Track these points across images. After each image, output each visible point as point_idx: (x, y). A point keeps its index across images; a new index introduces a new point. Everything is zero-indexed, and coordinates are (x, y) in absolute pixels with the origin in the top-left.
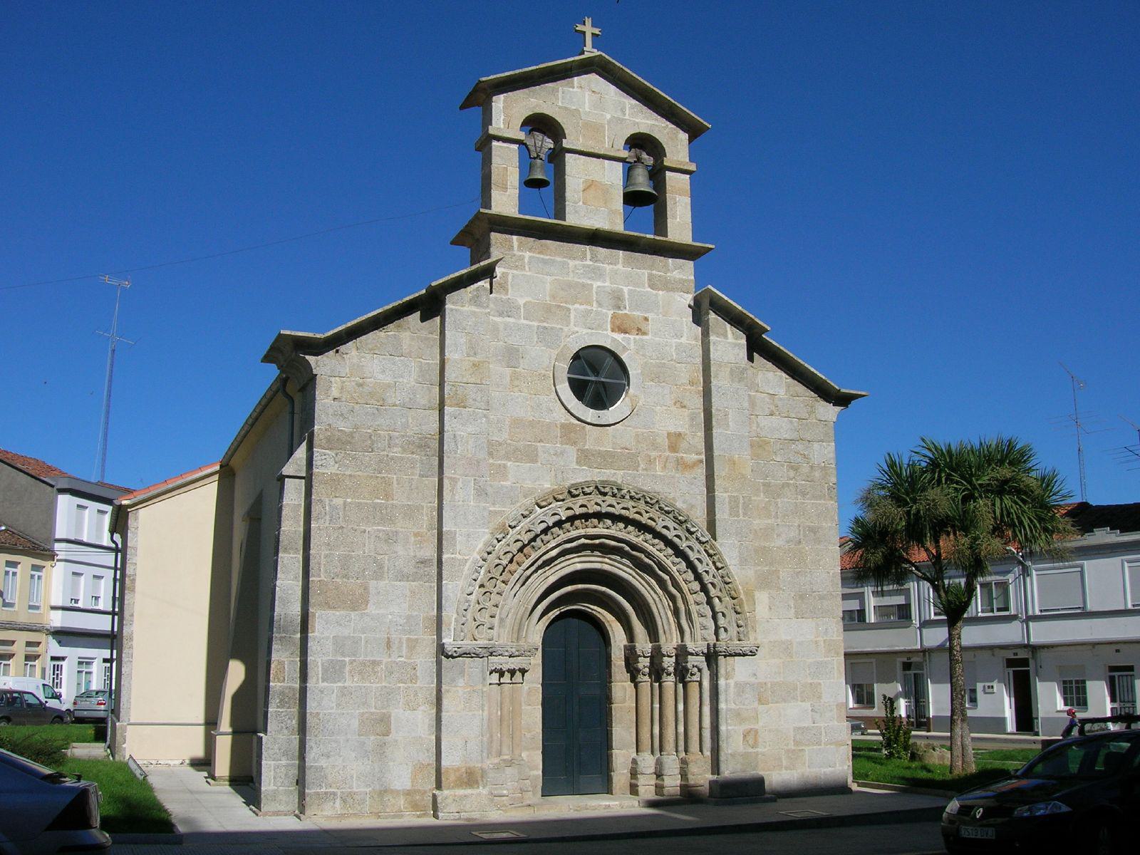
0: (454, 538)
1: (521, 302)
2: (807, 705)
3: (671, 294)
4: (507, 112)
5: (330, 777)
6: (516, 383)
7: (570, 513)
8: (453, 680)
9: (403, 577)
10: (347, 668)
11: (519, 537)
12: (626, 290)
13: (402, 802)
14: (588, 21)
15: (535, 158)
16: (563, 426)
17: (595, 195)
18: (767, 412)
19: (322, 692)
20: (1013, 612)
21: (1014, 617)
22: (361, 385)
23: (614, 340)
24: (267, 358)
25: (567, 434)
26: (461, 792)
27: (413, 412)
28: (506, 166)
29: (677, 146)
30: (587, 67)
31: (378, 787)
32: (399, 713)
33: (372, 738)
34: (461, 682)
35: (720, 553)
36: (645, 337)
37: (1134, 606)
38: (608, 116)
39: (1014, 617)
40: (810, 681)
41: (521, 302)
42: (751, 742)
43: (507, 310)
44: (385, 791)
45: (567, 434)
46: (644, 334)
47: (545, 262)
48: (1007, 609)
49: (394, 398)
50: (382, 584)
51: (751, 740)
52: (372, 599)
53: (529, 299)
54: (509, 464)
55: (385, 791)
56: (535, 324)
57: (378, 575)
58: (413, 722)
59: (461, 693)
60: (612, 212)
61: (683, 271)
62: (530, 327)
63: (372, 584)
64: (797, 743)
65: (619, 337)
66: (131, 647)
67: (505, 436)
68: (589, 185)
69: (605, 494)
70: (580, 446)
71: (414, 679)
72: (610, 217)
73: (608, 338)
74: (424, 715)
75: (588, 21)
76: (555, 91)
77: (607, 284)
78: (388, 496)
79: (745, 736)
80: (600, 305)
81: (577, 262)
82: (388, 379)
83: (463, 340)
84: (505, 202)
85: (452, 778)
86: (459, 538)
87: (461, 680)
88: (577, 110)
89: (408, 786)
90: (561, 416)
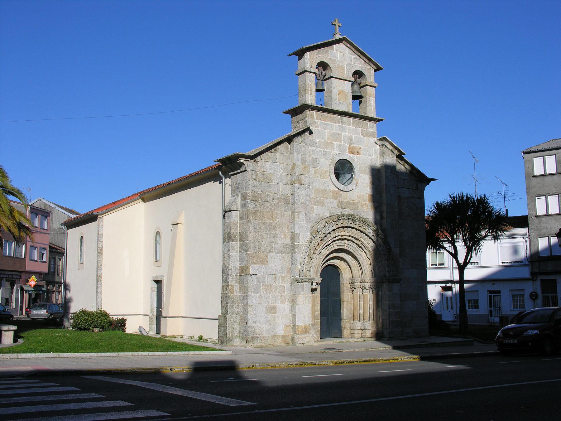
0: (299, 236)
1: (318, 140)
4: (310, 60)
5: (256, 331)
6: (316, 174)
7: (337, 226)
9: (281, 252)
10: (261, 288)
12: (353, 136)
13: (280, 340)
16: (333, 192)
17: (340, 93)
20: (446, 265)
21: (447, 268)
22: (263, 174)
23: (350, 157)
24: (219, 161)
26: (303, 336)
29: (370, 76)
30: (339, 41)
31: (272, 334)
32: (279, 305)
34: (302, 293)
37: (432, 265)
38: (346, 63)
39: (447, 268)
41: (318, 140)
43: (313, 144)
46: (360, 154)
48: (443, 264)
50: (272, 254)
57: (271, 252)
58: (284, 308)
60: (349, 104)
61: (372, 127)
62: (321, 151)
63: (269, 254)
65: (351, 155)
68: (340, 92)
69: (349, 219)
70: (339, 199)
71: (284, 292)
72: (347, 105)
73: (347, 156)
76: (327, 52)
77: (347, 134)
78: (274, 220)
80: (344, 142)
82: (271, 172)
84: (311, 99)
86: (301, 237)
89: (283, 334)
90: (332, 188)
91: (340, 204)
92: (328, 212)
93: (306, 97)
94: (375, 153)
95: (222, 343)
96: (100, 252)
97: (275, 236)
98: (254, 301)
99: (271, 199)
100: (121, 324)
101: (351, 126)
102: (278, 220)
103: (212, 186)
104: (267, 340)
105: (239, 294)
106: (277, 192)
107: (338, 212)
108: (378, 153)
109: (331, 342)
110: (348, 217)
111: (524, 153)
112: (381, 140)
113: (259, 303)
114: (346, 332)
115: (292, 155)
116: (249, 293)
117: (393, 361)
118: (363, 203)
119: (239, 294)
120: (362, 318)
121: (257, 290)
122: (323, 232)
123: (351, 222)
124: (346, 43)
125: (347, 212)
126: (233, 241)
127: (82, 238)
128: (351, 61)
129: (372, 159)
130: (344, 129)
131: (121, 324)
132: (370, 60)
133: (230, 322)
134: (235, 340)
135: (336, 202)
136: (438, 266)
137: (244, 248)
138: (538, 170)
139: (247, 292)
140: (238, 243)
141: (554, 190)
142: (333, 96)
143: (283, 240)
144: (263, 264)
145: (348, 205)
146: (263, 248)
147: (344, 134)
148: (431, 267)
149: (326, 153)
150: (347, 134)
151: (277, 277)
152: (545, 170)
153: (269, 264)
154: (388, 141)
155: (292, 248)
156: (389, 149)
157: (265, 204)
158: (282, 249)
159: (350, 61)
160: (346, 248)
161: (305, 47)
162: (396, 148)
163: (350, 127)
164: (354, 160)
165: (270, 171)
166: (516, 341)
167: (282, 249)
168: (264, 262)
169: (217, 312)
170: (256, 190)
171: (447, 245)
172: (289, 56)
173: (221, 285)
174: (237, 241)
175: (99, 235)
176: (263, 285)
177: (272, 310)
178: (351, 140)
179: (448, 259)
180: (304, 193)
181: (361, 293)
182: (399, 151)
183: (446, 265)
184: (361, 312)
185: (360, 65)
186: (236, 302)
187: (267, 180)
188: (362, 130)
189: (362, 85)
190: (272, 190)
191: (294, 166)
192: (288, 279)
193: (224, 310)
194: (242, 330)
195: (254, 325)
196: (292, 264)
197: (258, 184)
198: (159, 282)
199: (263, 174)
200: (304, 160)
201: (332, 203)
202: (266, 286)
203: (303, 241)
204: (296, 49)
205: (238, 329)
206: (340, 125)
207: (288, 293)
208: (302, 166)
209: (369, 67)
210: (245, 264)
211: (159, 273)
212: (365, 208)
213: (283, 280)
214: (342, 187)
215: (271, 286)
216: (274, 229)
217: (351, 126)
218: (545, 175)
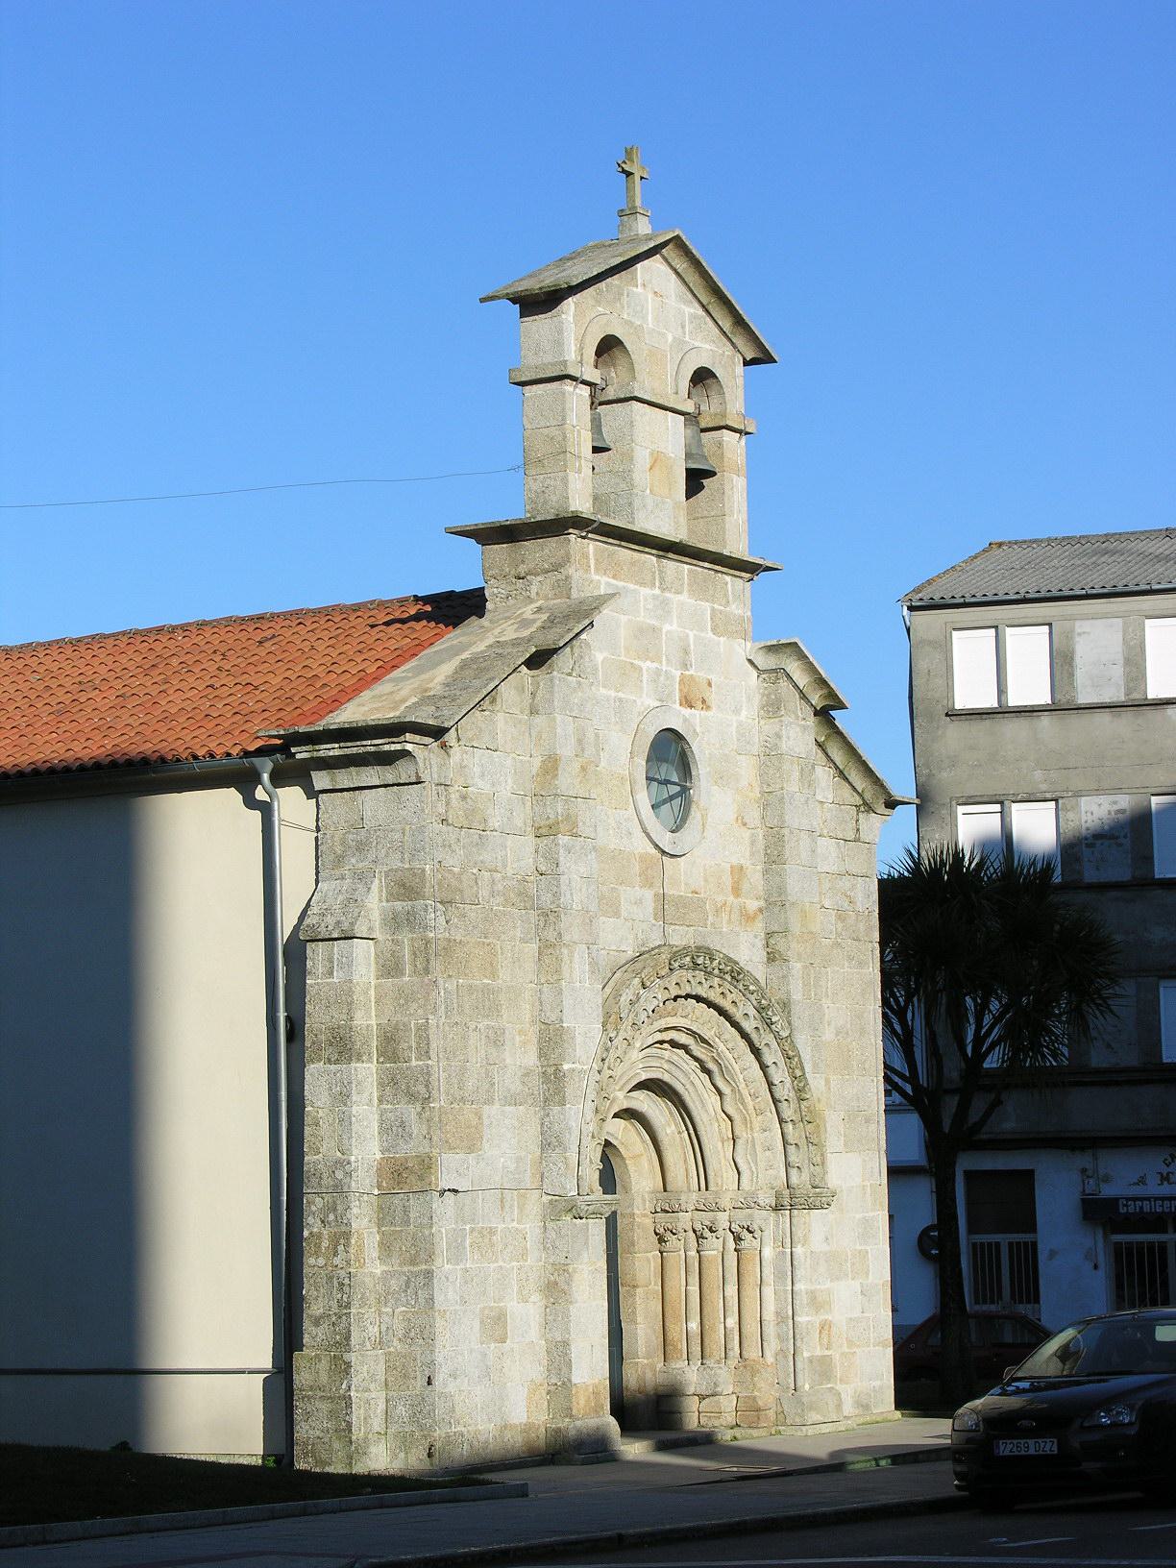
2: (856, 1285)
4: (573, 328)
12: (691, 635)
16: (643, 858)
32: (512, 1305)
36: (709, 713)
46: (708, 708)
56: (612, 693)
57: (489, 1101)
58: (526, 1313)
65: (687, 712)
71: (524, 1255)
73: (676, 718)
77: (675, 627)
78: (494, 976)
91: (665, 907)
93: (565, 482)
99: (484, 893)
101: (684, 597)
102: (504, 976)
105: (378, 1269)
108: (757, 700)
111: (911, 608)
115: (538, 720)
116: (438, 1262)
118: (720, 898)
119: (378, 1269)
120: (696, 1349)
124: (682, 265)
126: (359, 1059)
129: (740, 724)
132: (739, 321)
133: (360, 1377)
134: (373, 1450)
135: (648, 895)
137: (404, 1084)
138: (972, 690)
139: (430, 1257)
140: (373, 1066)
141: (1039, 779)
142: (636, 476)
143: (521, 1056)
144: (471, 1149)
147: (666, 627)
150: (675, 627)
152: (1002, 690)
153: (486, 1146)
154: (802, 657)
155: (553, 1084)
156: (796, 686)
157: (473, 913)
158: (516, 1086)
160: (666, 1078)
162: (822, 682)
166: (1049, 1446)
170: (449, 862)
172: (482, 300)
176: (472, 1230)
181: (693, 1253)
182: (832, 694)
184: (694, 1325)
185: (710, 347)
186: (372, 1300)
188: (713, 610)
191: (551, 766)
192: (535, 1203)
195: (451, 1388)
196: (546, 1146)
201: (639, 902)
204: (533, 285)
205: (382, 1406)
206: (657, 591)
207: (534, 1260)
208: (577, 766)
209: (728, 349)
210: (407, 1150)
212: (725, 917)
215: (492, 1232)
216: (494, 1010)
217: (684, 597)
218: (1002, 712)
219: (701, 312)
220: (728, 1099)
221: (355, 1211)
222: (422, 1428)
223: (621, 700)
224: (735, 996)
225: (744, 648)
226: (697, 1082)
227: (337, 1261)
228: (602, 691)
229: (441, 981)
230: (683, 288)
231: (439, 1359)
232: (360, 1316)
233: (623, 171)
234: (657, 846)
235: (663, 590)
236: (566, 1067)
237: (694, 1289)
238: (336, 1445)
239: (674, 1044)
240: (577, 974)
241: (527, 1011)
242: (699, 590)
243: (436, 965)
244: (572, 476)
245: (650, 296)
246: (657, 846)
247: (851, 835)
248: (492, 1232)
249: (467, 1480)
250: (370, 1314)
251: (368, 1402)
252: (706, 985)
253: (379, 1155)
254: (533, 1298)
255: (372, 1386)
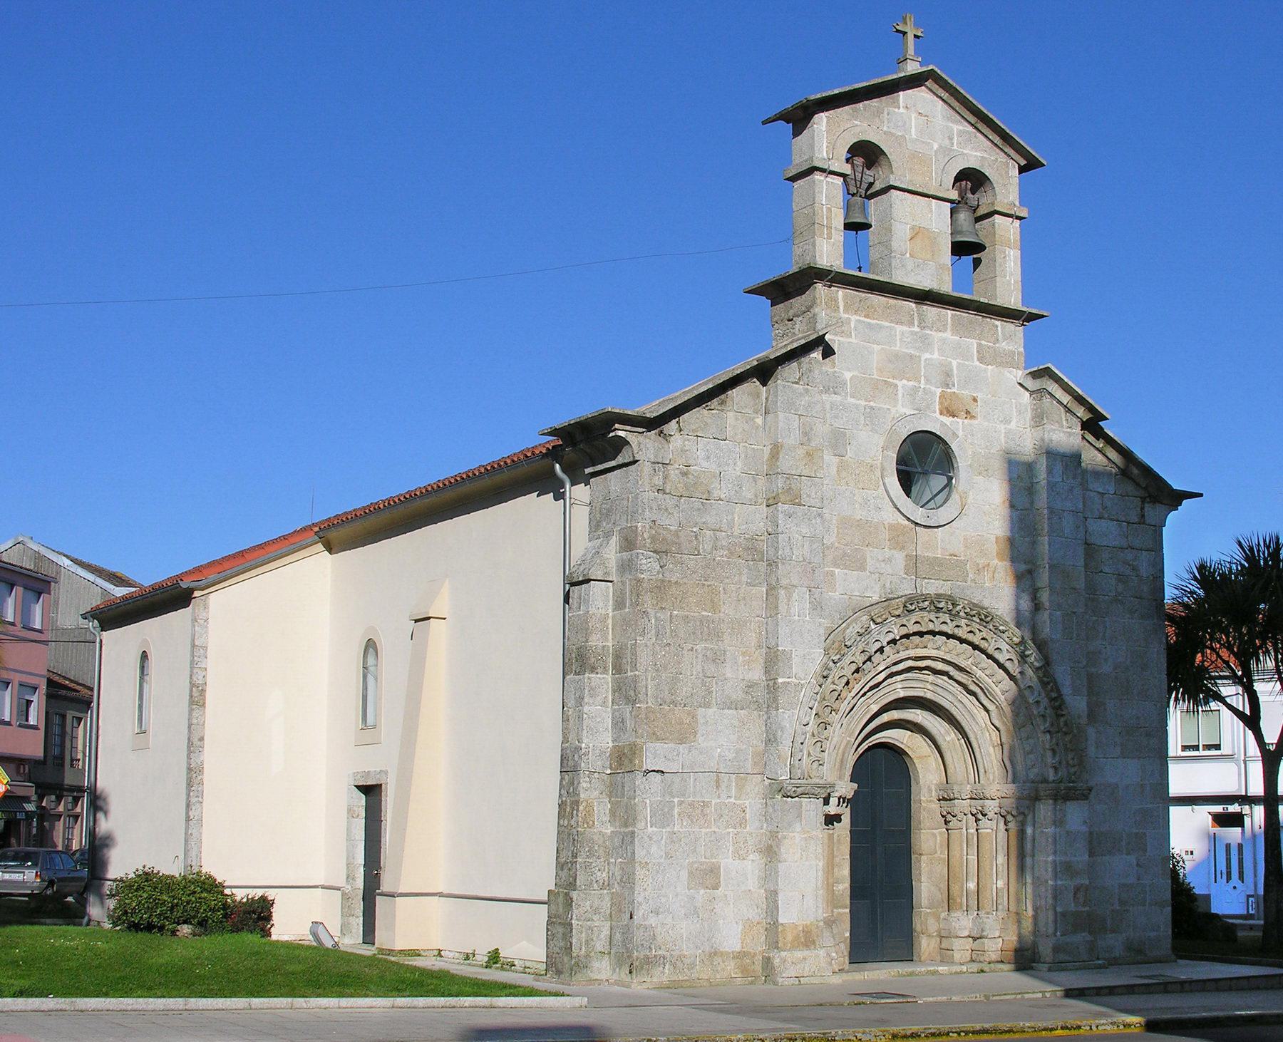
2: (1132, 859)
3: (1001, 369)
4: (828, 137)
5: (659, 938)
6: (844, 474)
7: (904, 631)
8: (790, 825)
11: (853, 659)
12: (954, 363)
14: (910, 20)
15: (853, 195)
16: (892, 528)
18: (1097, 514)
19: (651, 839)
20: (1225, 750)
21: (1229, 757)
22: (685, 474)
23: (943, 425)
25: (897, 539)
26: (799, 954)
27: (738, 508)
28: (827, 196)
30: (914, 81)
32: (727, 862)
33: (702, 892)
34: (798, 827)
35: (1055, 683)
36: (973, 422)
37: (1185, 748)
38: (936, 146)
39: (1229, 757)
40: (1135, 831)
41: (848, 375)
42: (1081, 900)
44: (715, 953)
45: (897, 539)
46: (973, 417)
47: (870, 326)
48: (1218, 747)
49: (721, 491)
50: (710, 711)
51: (1081, 895)
52: (701, 729)
53: (855, 373)
54: (837, 571)
55: (715, 953)
56: (863, 403)
58: (742, 871)
59: (797, 840)
61: (1010, 337)
62: (857, 407)
63: (701, 711)
64: (1122, 903)
65: (948, 420)
66: (201, 783)
67: (833, 539)
68: (917, 233)
71: (743, 823)
72: (935, 271)
73: (935, 423)
74: (752, 865)
75: (910, 20)
76: (879, 113)
78: (715, 608)
79: (1075, 894)
80: (927, 380)
81: (905, 328)
82: (711, 466)
83: (796, 424)
84: (829, 251)
85: (790, 938)
87: (798, 825)
88: (903, 136)
89: (738, 948)
91: (914, 565)
92: (877, 588)
93: (814, 245)
94: (1020, 413)
95: (559, 972)
96: (197, 698)
97: (717, 658)
98: (654, 849)
99: (708, 547)
100: (257, 914)
102: (728, 610)
103: (533, 509)
104: (693, 965)
106: (725, 527)
107: (907, 589)
109: (880, 974)
110: (935, 604)
112: (1036, 375)
113: (669, 856)
114: (926, 945)
116: (640, 825)
117: (1066, 1032)
118: (982, 562)
119: (609, 830)
121: (663, 817)
122: (861, 646)
123: (946, 618)
125: (932, 587)
127: (144, 656)
128: (951, 139)
129: (1008, 432)
130: (926, 343)
131: (257, 914)
132: (1005, 137)
133: (582, 910)
134: (596, 964)
135: (899, 557)
136: (1202, 752)
140: (609, 677)
143: (743, 670)
145: (937, 567)
146: (684, 691)
147: (927, 355)
148: (1180, 753)
149: (871, 414)
150: (936, 356)
151: (725, 778)
153: (700, 739)
155: (769, 694)
156: (1060, 402)
157: (690, 561)
158: (739, 695)
159: (947, 142)
160: (929, 695)
161: (813, 97)
162: (1080, 400)
163: (945, 340)
164: (955, 435)
165: (705, 464)
167: (739, 695)
168: (685, 735)
169: (543, 880)
170: (664, 521)
171: (1230, 691)
172: (764, 123)
173: (556, 801)
174: (605, 671)
175: (196, 651)
176: (681, 803)
177: (708, 876)
178: (948, 374)
179: (1232, 731)
180: (805, 530)
181: (972, 831)
182: (1091, 409)
183: (1225, 750)
184: (972, 885)
186: (601, 852)
187: (697, 492)
188: (979, 345)
189: (981, 212)
190: (710, 519)
192: (756, 786)
193: (564, 874)
194: (618, 936)
195: (652, 921)
197: (670, 501)
198: (371, 791)
199: (685, 474)
200: (805, 434)
202: (691, 805)
203: (801, 675)
206: (916, 329)
208: (801, 452)
210: (627, 739)
211: (371, 765)
212: (987, 576)
213: (740, 788)
214: (919, 514)
215: (705, 805)
216: (717, 635)
219: (971, 129)
220: (993, 714)
221: (584, 785)
222: (627, 949)
223: (872, 408)
224: (989, 635)
225: (1019, 374)
226: (965, 701)
227: (572, 822)
228: (852, 400)
229: (652, 613)
230: (951, 111)
231: (639, 898)
232: (587, 866)
233: (898, 31)
234: (908, 519)
235: (923, 328)
236: (780, 680)
237: (973, 858)
238: (566, 959)
239: (936, 672)
240: (795, 609)
241: (752, 638)
242: (958, 328)
243: (648, 602)
244: (818, 241)
245: (913, 116)
246: (908, 519)
247: (1134, 517)
248: (705, 805)
249: (1216, 916)
250: (597, 863)
251: (591, 929)
252: (952, 625)
253: (611, 744)
254: (751, 857)
255: (595, 918)
